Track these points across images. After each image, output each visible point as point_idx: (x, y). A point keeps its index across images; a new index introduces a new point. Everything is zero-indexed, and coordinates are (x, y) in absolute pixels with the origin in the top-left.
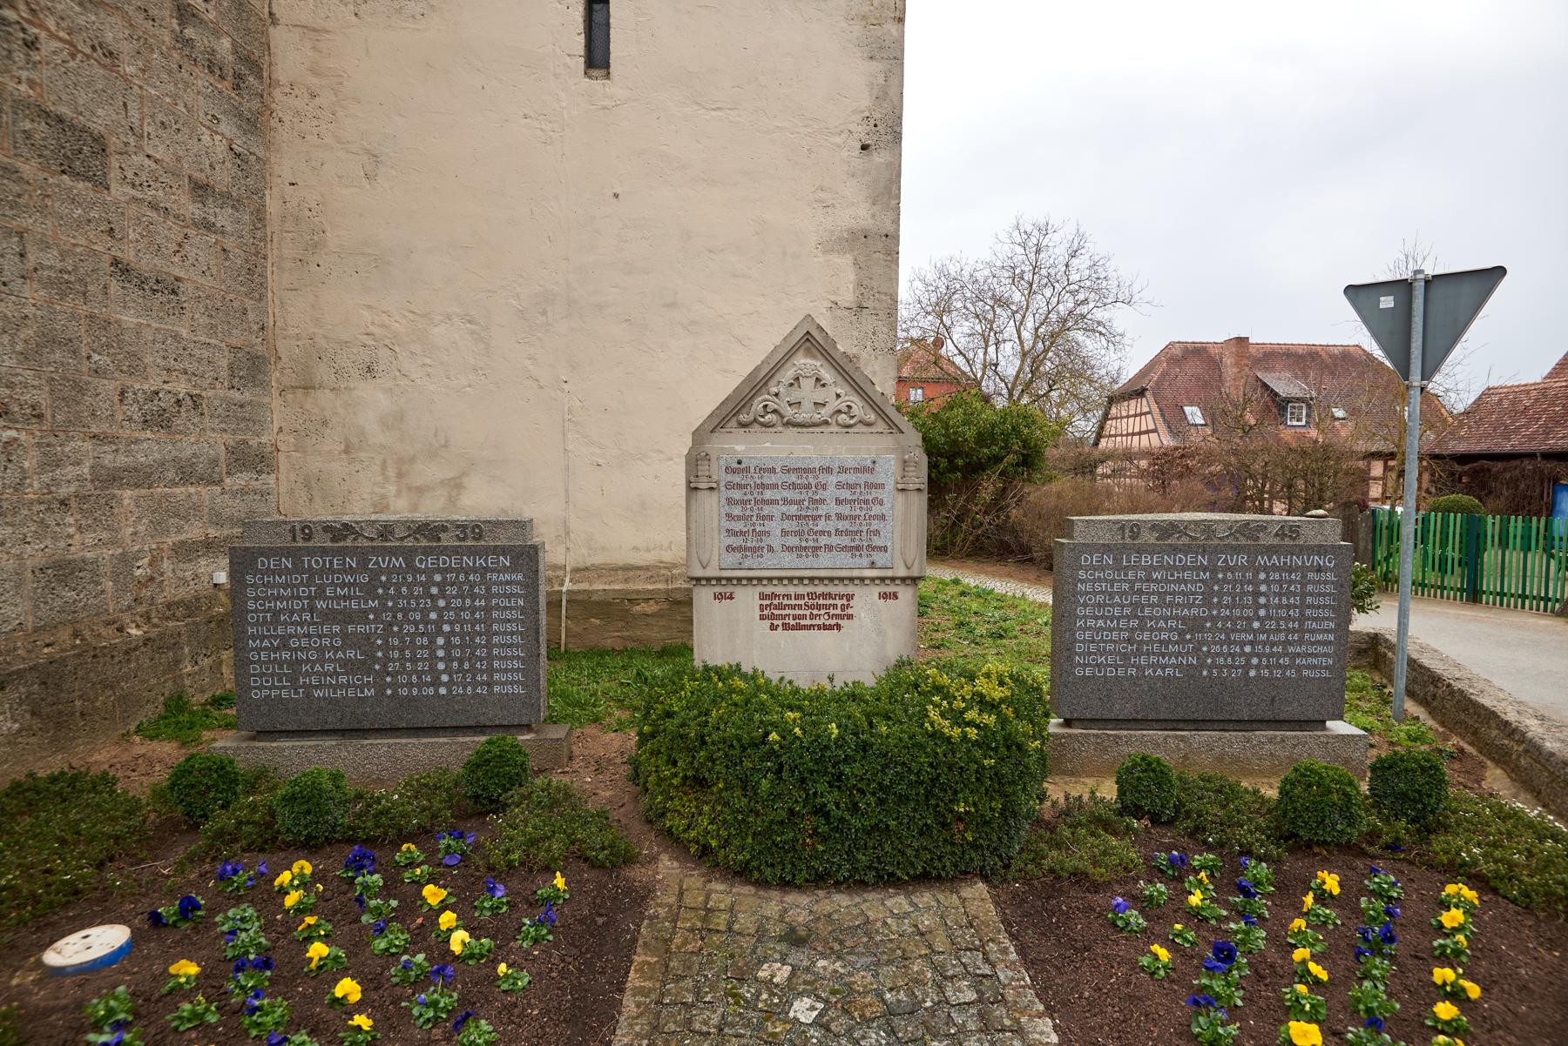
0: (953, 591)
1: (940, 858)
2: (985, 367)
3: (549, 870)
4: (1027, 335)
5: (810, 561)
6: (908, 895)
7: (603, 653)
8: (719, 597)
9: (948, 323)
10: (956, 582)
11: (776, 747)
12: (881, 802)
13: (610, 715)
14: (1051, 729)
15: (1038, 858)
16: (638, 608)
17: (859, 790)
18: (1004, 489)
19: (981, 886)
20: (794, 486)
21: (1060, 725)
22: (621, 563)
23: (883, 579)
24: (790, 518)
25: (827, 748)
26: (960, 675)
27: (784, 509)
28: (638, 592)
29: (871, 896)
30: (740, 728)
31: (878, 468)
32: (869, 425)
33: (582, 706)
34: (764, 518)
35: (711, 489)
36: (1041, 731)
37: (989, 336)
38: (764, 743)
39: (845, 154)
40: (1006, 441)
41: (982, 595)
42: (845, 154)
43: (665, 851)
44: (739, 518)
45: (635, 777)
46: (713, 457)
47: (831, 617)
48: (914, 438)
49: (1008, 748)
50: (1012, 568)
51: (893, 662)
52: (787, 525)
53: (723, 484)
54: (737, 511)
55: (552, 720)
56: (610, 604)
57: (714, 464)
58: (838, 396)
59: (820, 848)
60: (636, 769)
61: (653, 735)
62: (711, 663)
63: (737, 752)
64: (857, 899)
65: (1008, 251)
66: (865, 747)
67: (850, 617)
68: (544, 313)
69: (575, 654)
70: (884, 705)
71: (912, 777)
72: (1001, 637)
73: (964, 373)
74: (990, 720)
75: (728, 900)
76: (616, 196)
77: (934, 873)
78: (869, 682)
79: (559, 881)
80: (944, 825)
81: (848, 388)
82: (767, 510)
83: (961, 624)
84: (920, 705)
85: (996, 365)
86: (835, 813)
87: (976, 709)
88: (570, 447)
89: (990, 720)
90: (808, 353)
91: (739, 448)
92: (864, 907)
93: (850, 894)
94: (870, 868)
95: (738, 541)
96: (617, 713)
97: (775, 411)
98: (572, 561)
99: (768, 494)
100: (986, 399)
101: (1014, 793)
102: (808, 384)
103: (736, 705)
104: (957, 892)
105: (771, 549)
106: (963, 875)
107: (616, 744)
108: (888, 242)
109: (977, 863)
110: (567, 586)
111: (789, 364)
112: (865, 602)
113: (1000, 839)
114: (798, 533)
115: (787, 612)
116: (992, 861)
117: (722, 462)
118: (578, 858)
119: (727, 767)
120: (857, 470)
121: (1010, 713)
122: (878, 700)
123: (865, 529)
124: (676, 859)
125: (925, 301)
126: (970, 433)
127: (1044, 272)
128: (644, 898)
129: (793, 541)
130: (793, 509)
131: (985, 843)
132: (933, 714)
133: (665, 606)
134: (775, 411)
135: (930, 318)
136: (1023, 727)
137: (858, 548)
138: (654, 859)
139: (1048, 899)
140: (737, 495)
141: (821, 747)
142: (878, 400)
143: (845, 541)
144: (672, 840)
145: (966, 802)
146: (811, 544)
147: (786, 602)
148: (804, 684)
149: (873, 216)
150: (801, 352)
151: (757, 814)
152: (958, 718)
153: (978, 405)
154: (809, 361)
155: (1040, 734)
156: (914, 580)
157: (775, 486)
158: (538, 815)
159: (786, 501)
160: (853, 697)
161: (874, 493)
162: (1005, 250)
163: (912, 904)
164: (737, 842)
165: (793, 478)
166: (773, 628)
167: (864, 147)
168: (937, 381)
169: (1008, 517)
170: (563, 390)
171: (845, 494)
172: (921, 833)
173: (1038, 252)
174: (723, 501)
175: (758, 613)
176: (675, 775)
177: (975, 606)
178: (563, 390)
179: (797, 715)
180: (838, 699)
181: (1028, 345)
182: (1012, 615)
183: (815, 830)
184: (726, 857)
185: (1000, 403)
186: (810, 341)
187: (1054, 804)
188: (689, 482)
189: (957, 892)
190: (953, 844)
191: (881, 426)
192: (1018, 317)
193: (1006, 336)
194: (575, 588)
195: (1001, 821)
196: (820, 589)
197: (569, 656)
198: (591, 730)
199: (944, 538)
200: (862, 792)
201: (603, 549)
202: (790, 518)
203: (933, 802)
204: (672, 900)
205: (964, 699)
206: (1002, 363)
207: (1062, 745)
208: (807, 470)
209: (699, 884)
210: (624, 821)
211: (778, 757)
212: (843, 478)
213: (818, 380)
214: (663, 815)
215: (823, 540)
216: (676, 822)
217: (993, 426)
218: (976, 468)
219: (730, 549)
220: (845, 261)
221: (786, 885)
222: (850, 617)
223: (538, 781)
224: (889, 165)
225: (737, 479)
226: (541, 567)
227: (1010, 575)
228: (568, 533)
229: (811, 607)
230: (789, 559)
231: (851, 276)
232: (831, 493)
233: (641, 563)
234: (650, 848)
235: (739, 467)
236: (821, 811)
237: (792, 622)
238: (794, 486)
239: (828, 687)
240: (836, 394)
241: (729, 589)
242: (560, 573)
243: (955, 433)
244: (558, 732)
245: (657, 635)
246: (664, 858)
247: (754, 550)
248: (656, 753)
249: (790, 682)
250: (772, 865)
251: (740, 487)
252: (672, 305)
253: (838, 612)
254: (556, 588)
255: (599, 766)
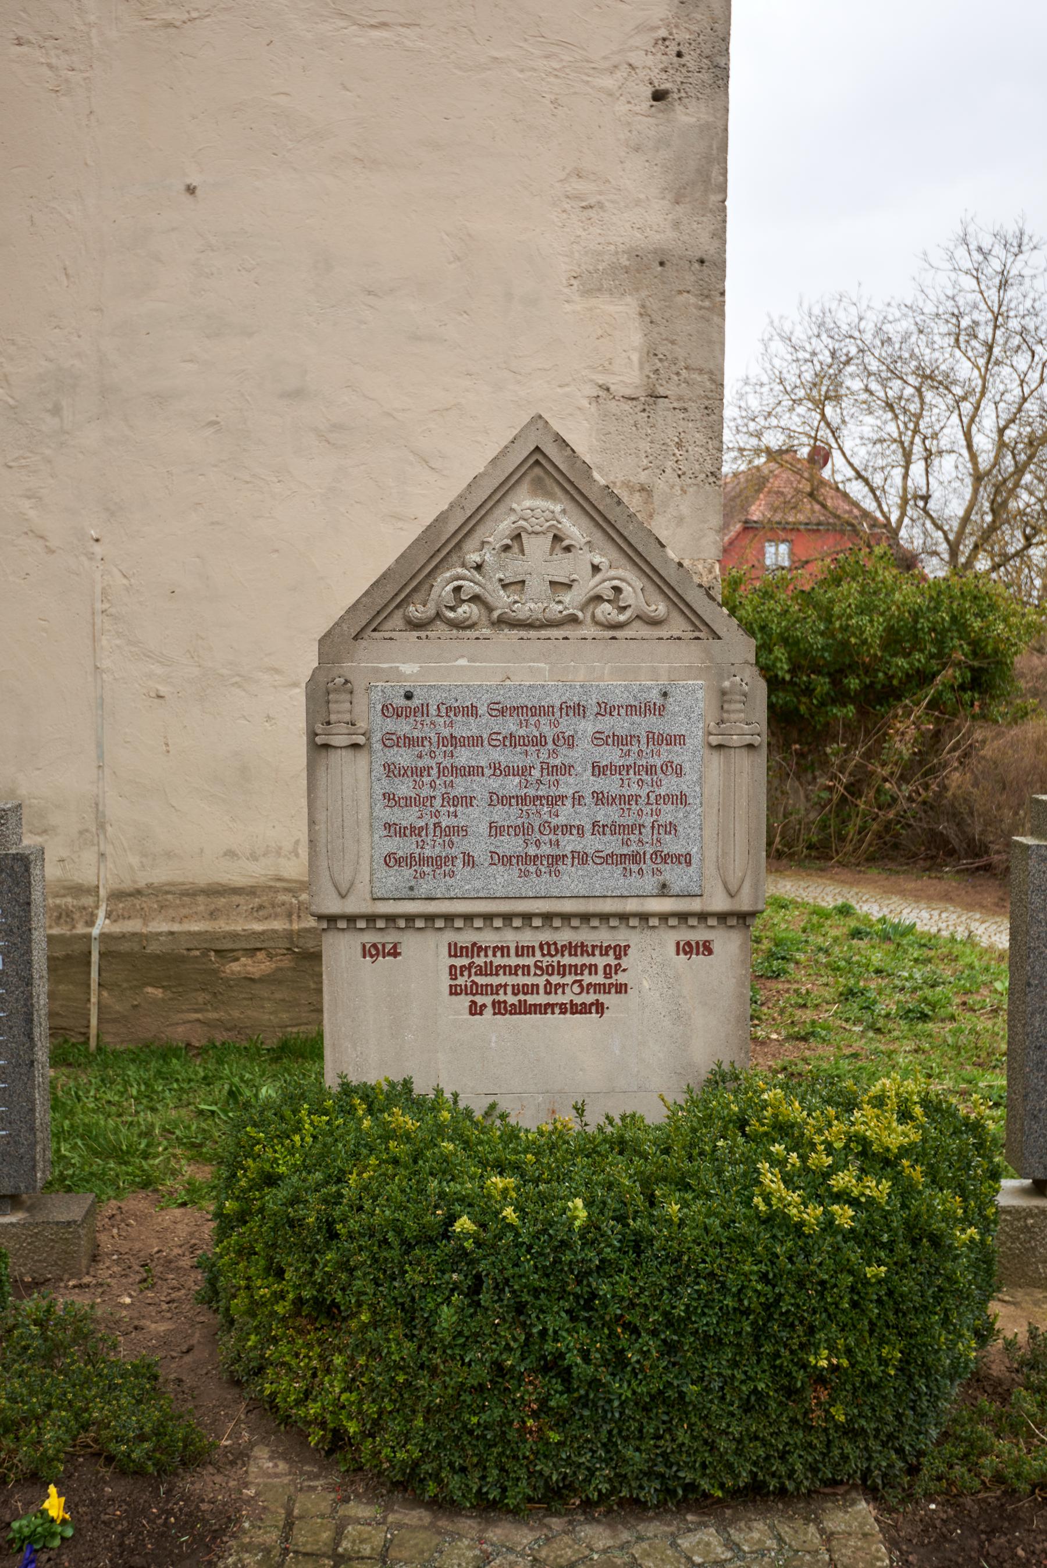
0: (837, 929)
1: (783, 1456)
2: (905, 501)
3: (36, 1482)
4: (984, 442)
5: (544, 883)
6: (722, 1528)
7: (167, 1052)
8: (372, 952)
9: (835, 421)
10: (845, 911)
11: (469, 1245)
12: (670, 1348)
13: (174, 1173)
14: (1003, 1200)
15: (973, 1452)
16: (235, 967)
17: (627, 1326)
18: (937, 735)
19: (863, 1506)
20: (512, 740)
21: (1025, 1192)
22: (202, 881)
23: (683, 917)
24: (505, 800)
25: (564, 1245)
26: (828, 1101)
27: (494, 784)
28: (234, 936)
29: (653, 1529)
30: (401, 1207)
31: (672, 706)
32: (655, 623)
33: (121, 1156)
34: (456, 801)
35: (355, 746)
36: (981, 1208)
37: (912, 445)
38: (446, 1236)
39: (621, 108)
40: (940, 643)
41: (894, 935)
42: (621, 108)
43: (264, 1441)
44: (409, 802)
45: (212, 1294)
46: (359, 685)
47: (585, 989)
48: (741, 648)
49: (915, 1243)
50: (949, 881)
51: (704, 1075)
52: (501, 815)
53: (377, 737)
54: (404, 788)
55: (64, 1185)
56: (183, 959)
57: (361, 701)
58: (596, 569)
59: (554, 1437)
60: (212, 1282)
61: (242, 1217)
62: (354, 1080)
63: (395, 1253)
64: (625, 1536)
65: (946, 284)
66: (638, 1244)
67: (621, 989)
68: (56, 411)
69: (117, 1055)
70: (677, 1160)
71: (729, 1302)
72: (924, 1017)
73: (866, 514)
74: (878, 1189)
75: (379, 1537)
76: (191, 190)
77: (773, 1484)
78: (655, 1115)
79: (54, 1505)
80: (790, 1392)
81: (614, 554)
82: (461, 786)
83: (849, 994)
84: (746, 1160)
85: (926, 498)
86: (582, 1370)
87: (854, 1169)
88: (106, 664)
89: (878, 1189)
90: (539, 488)
91: (408, 668)
92: (637, 1551)
93: (611, 1526)
94: (649, 1474)
95: (406, 846)
96: (188, 1170)
97: (476, 599)
98: (109, 879)
99: (464, 757)
100: (908, 562)
101: (925, 1330)
102: (537, 547)
103: (396, 1162)
104: (817, 1521)
105: (469, 860)
106: (830, 1486)
107: (182, 1231)
108: (707, 272)
109: (856, 1463)
110: (101, 925)
111: (501, 509)
112: (651, 962)
113: (898, 1417)
114: (522, 830)
115: (501, 979)
116: (885, 1459)
117: (376, 696)
118: (92, 1456)
119: (376, 1283)
120: (631, 710)
121: (917, 1174)
122: (667, 1151)
123: (648, 821)
124: (284, 1457)
125: (792, 379)
126: (873, 628)
127: (1014, 324)
128: (217, 1534)
129: (511, 845)
130: (512, 785)
131: (870, 1427)
132: (771, 1179)
133: (286, 963)
134: (476, 599)
135: (801, 410)
136: (946, 1201)
137: (635, 858)
138: (241, 1456)
139: (991, 1532)
140: (404, 757)
141: (552, 1242)
142: (671, 575)
143: (611, 844)
144: (277, 1419)
145: (832, 1348)
146: (546, 850)
147: (499, 961)
148: (529, 1119)
149: (676, 224)
150: (525, 487)
151: (434, 1372)
152: (817, 1187)
153: (888, 575)
154: (541, 503)
155: (981, 1214)
156: (744, 918)
157: (476, 741)
158: (21, 1375)
159: (497, 769)
160: (621, 1145)
161: (666, 753)
162: (941, 282)
163: (731, 1545)
164: (395, 1426)
165: (511, 725)
166: (475, 1010)
167: (659, 96)
168: (814, 529)
169: (945, 788)
170: (91, 556)
171: (611, 755)
172: (747, 1408)
173: (1004, 285)
174: (379, 770)
175: (446, 981)
176: (281, 1296)
177: (877, 958)
178: (91, 556)
179: (511, 1181)
180: (592, 1149)
181: (985, 461)
182: (948, 974)
183: (543, 1402)
184: (376, 1454)
185: (935, 569)
186: (543, 465)
187: (1010, 1345)
188: (312, 734)
189: (817, 1521)
190: (809, 1429)
191: (678, 626)
192: (967, 407)
193: (944, 443)
194: (117, 928)
195: (901, 1384)
196: (565, 936)
197: (104, 1057)
198: (137, 1203)
199: (824, 826)
200: (635, 1331)
201: (169, 855)
202: (505, 800)
203: (768, 1348)
204: (272, 1537)
205: (830, 1150)
206: (937, 493)
207: (1027, 1229)
208: (536, 711)
209: (325, 1507)
210: (189, 1381)
211: (472, 1263)
212: (606, 724)
213: (557, 538)
214: (260, 1371)
215: (570, 844)
216: (284, 1387)
217: (916, 615)
218: (881, 696)
219: (391, 860)
220: (622, 309)
221: (489, 1508)
222: (621, 989)
223: (28, 1305)
224: (705, 128)
225: (404, 727)
226: (36, 896)
227: (947, 897)
228: (101, 826)
229: (549, 970)
230: (503, 879)
231: (634, 338)
232: (582, 754)
233: (239, 881)
234: (235, 1435)
235: (408, 704)
236: (553, 1366)
237: (511, 999)
238: (512, 740)
239: (575, 1126)
240: (592, 564)
241: (390, 938)
242: (88, 901)
243: (844, 629)
244: (69, 1209)
245: (269, 1017)
246: (261, 1453)
247: (437, 862)
248: (246, 1252)
249: (503, 1117)
250: (463, 1470)
251: (410, 742)
252: (297, 394)
253: (599, 979)
254: (81, 929)
255: (148, 1273)
